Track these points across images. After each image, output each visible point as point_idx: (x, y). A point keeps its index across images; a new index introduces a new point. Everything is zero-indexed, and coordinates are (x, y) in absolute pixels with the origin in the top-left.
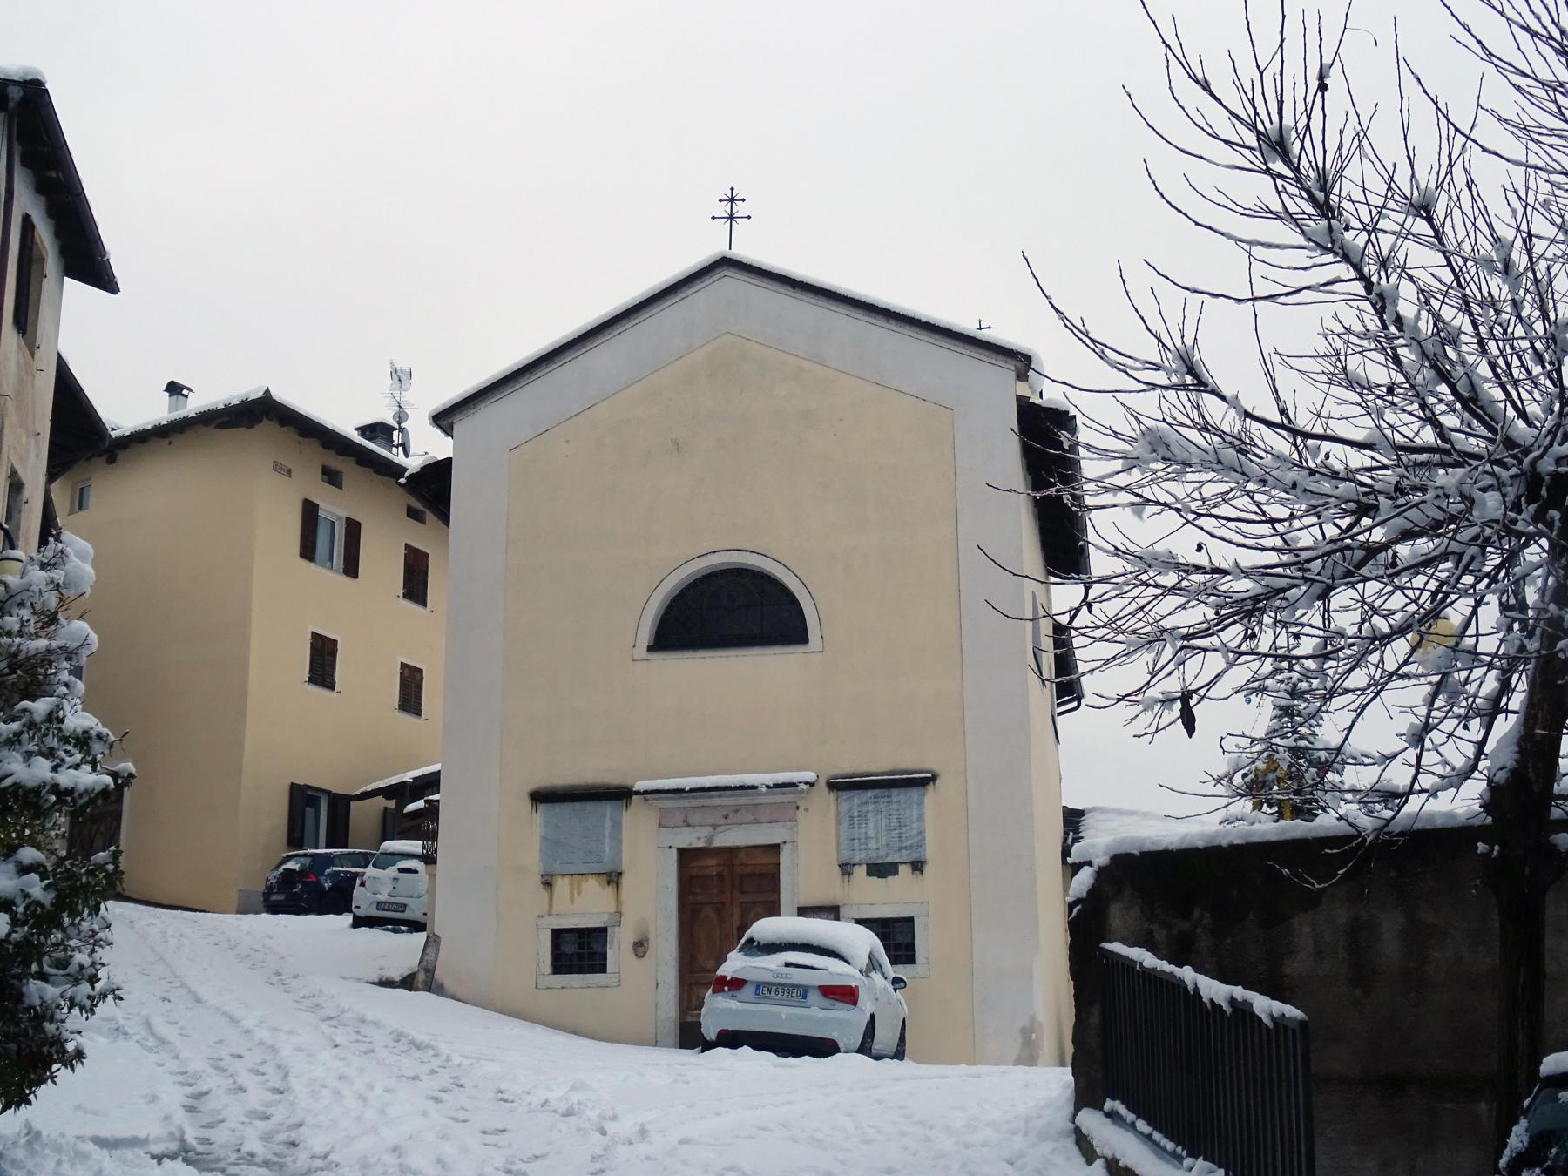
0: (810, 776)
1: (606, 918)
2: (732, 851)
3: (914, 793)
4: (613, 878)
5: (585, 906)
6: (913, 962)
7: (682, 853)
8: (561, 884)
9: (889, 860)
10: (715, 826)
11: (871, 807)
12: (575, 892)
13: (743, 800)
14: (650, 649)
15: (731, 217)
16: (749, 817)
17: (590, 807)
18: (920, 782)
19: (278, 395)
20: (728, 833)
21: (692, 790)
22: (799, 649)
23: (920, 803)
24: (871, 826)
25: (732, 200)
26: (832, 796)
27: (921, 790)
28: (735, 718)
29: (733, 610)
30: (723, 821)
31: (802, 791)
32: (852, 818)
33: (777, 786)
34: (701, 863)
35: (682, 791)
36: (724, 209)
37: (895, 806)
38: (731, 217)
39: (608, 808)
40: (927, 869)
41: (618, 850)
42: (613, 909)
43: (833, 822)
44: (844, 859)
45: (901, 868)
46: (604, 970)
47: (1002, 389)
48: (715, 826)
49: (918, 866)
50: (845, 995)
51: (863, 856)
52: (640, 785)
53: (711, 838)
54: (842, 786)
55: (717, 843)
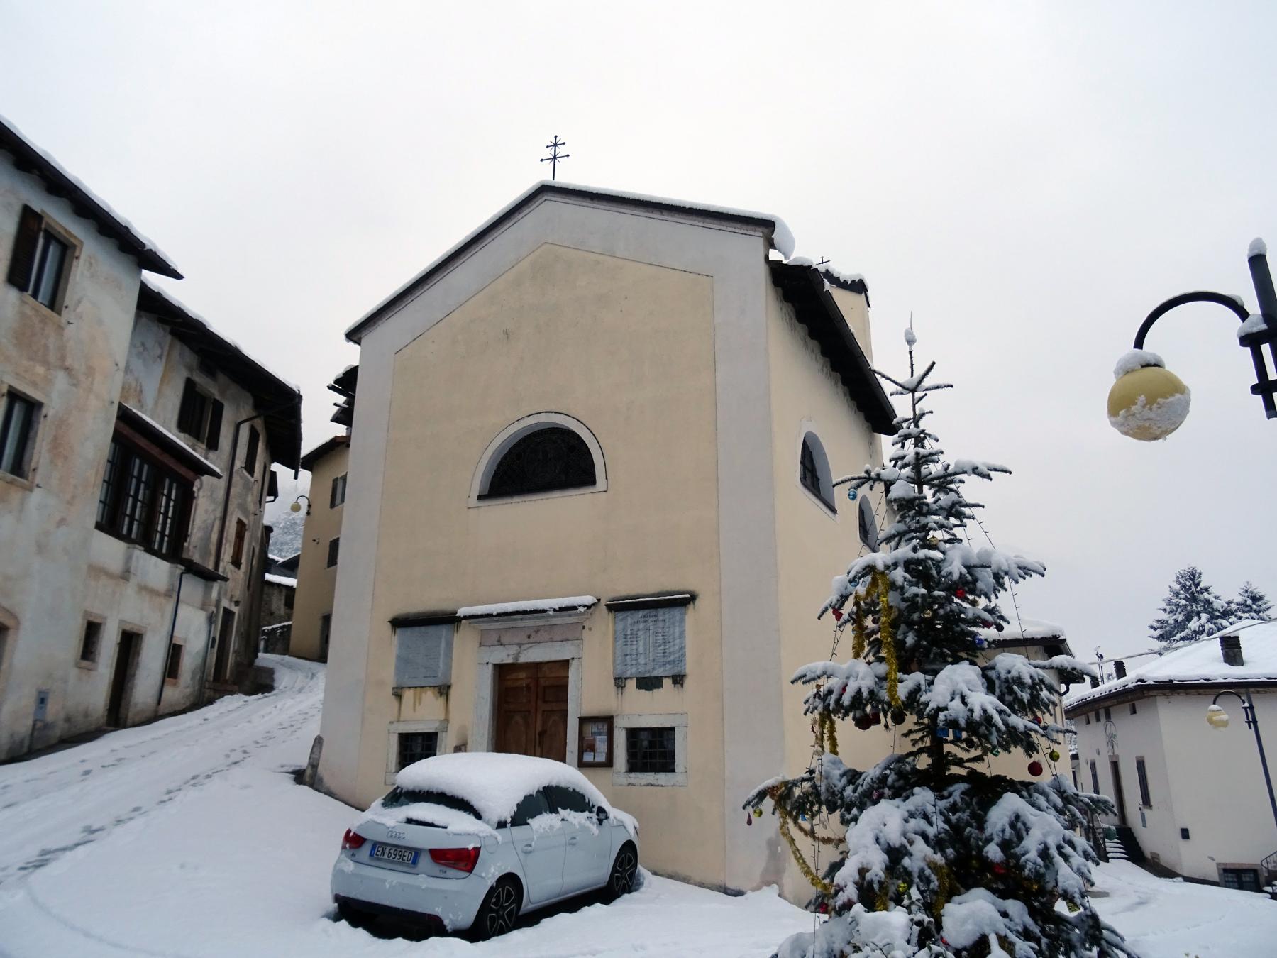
0: (589, 600)
1: (437, 724)
2: (537, 666)
3: (677, 612)
4: (444, 690)
5: (422, 714)
6: (673, 771)
8: (408, 695)
9: (655, 674)
10: (520, 645)
11: (641, 626)
12: (417, 701)
13: (540, 622)
14: (480, 497)
16: (547, 637)
17: (431, 630)
18: (684, 601)
20: (531, 651)
21: (499, 615)
22: (587, 490)
23: (682, 621)
24: (641, 643)
25: (556, 145)
26: (611, 616)
29: (545, 461)
30: (527, 640)
31: (582, 614)
32: (626, 636)
33: (562, 609)
34: (514, 676)
35: (489, 615)
37: (661, 624)
38: (555, 158)
39: (443, 631)
40: (687, 682)
41: (449, 667)
42: (442, 717)
43: (611, 639)
44: (619, 672)
47: (746, 252)
48: (520, 645)
49: (678, 680)
50: (464, 859)
51: (634, 670)
52: (462, 612)
53: (517, 656)
54: (619, 607)
55: (522, 660)
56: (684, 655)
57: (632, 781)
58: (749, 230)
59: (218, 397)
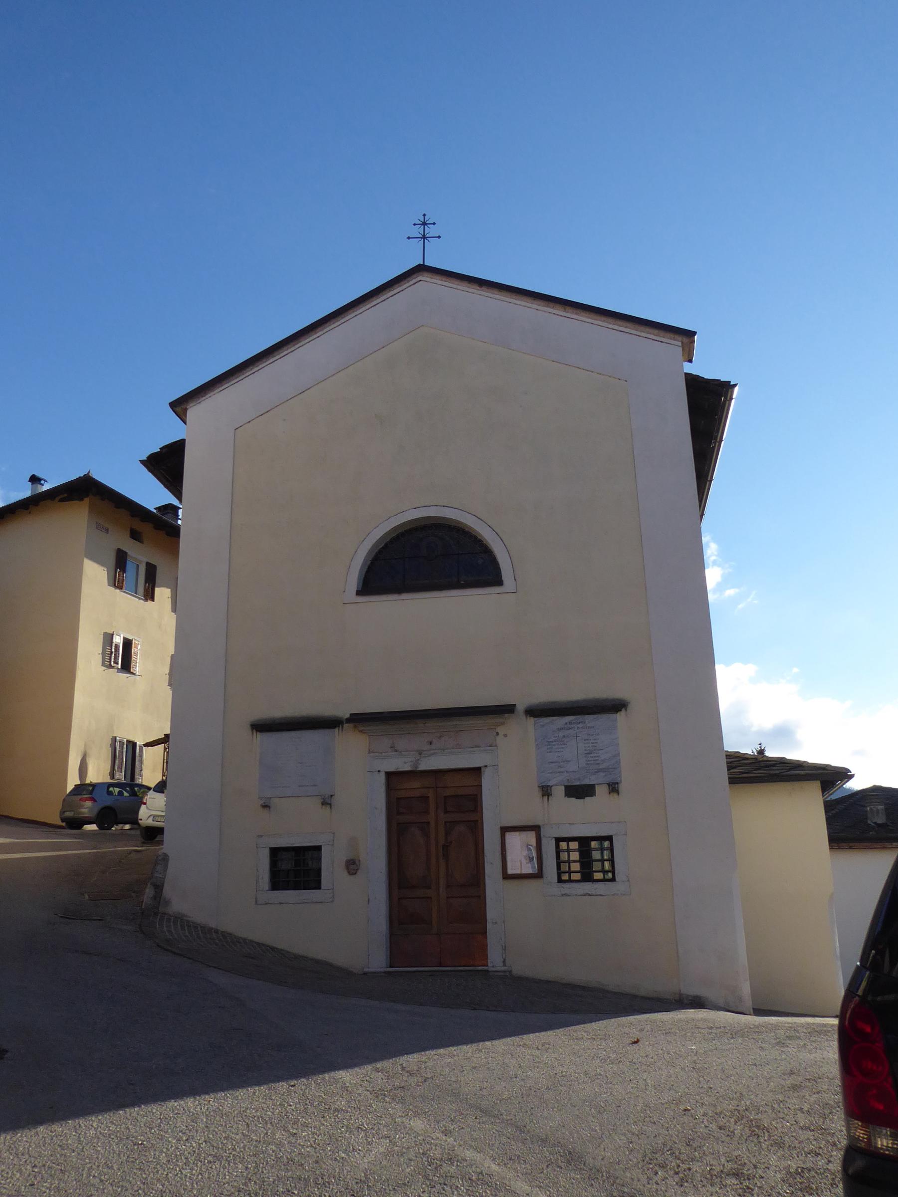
5: (297, 827)
7: (389, 775)
9: (587, 782)
15: (424, 237)
18: (616, 706)
19: (98, 476)
27: (612, 716)
28: (435, 643)
29: (429, 557)
36: (417, 231)
38: (424, 237)
40: (622, 788)
45: (597, 788)
46: (318, 887)
49: (614, 788)
55: (422, 767)
56: (618, 762)
57: (567, 891)
58: (666, 338)
59: (734, 396)
